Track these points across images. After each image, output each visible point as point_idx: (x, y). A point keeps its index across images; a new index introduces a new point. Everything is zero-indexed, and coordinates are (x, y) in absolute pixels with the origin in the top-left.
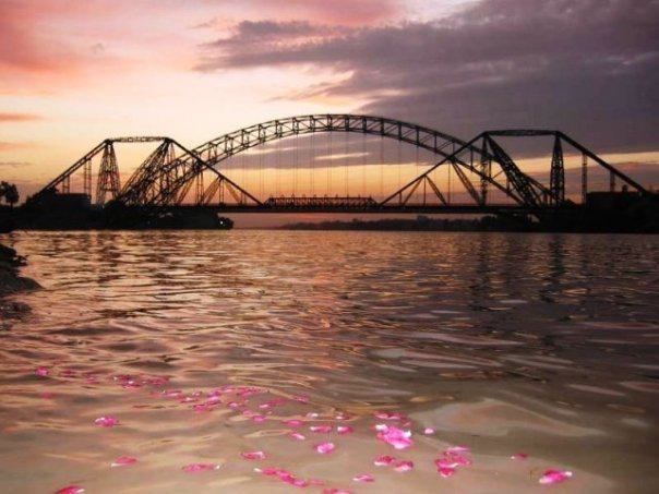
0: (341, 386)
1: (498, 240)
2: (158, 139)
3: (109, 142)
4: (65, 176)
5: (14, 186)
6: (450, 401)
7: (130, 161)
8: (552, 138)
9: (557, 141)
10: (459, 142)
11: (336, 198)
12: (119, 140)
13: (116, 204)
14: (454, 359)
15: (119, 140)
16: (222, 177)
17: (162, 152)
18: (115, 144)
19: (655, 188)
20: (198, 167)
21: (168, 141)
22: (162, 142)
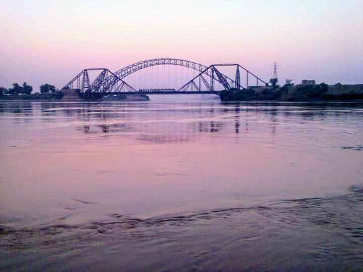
0: (298, 202)
1: (121, 78)
2: (102, 69)
3: (86, 70)
4: (71, 82)
5: (53, 86)
6: (330, 200)
7: (93, 76)
8: (236, 66)
9: (238, 67)
10: (247, 74)
11: (312, 114)
12: (89, 69)
13: (89, 91)
14: (97, 102)
15: (89, 69)
16: (124, 83)
17: (103, 74)
18: (88, 71)
19: (362, 92)
20: (117, 78)
21: (105, 70)
22: (103, 70)
